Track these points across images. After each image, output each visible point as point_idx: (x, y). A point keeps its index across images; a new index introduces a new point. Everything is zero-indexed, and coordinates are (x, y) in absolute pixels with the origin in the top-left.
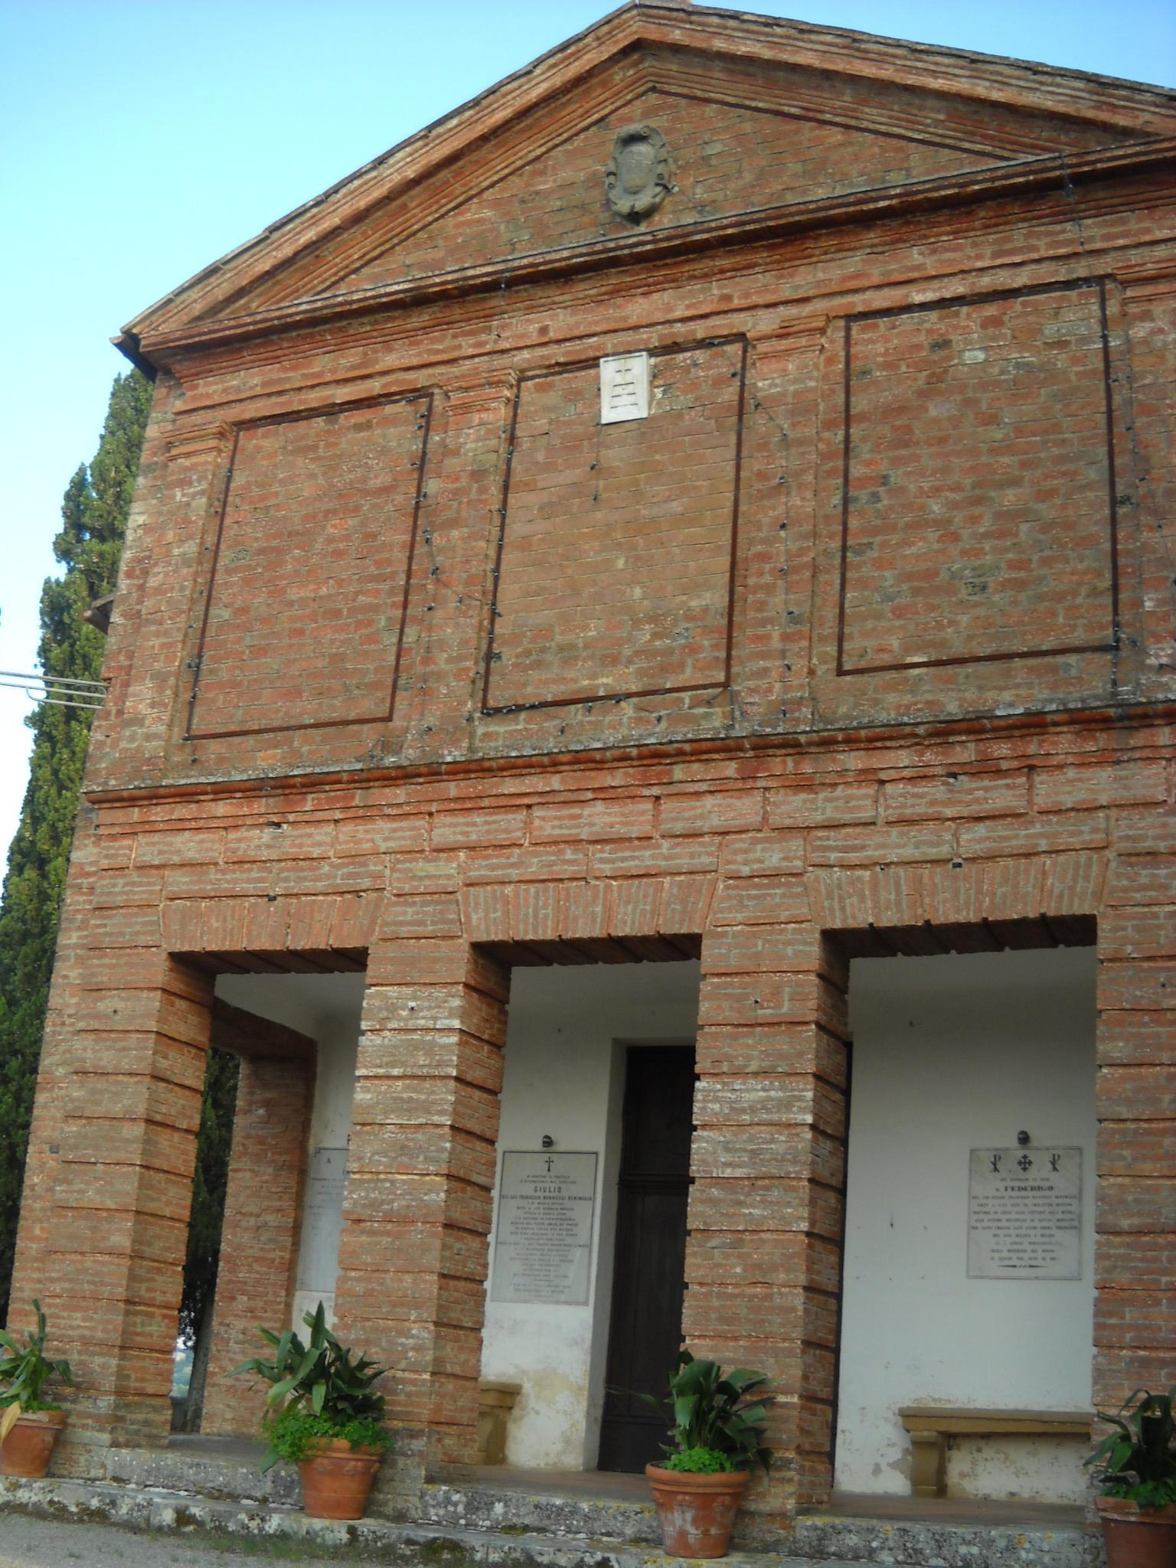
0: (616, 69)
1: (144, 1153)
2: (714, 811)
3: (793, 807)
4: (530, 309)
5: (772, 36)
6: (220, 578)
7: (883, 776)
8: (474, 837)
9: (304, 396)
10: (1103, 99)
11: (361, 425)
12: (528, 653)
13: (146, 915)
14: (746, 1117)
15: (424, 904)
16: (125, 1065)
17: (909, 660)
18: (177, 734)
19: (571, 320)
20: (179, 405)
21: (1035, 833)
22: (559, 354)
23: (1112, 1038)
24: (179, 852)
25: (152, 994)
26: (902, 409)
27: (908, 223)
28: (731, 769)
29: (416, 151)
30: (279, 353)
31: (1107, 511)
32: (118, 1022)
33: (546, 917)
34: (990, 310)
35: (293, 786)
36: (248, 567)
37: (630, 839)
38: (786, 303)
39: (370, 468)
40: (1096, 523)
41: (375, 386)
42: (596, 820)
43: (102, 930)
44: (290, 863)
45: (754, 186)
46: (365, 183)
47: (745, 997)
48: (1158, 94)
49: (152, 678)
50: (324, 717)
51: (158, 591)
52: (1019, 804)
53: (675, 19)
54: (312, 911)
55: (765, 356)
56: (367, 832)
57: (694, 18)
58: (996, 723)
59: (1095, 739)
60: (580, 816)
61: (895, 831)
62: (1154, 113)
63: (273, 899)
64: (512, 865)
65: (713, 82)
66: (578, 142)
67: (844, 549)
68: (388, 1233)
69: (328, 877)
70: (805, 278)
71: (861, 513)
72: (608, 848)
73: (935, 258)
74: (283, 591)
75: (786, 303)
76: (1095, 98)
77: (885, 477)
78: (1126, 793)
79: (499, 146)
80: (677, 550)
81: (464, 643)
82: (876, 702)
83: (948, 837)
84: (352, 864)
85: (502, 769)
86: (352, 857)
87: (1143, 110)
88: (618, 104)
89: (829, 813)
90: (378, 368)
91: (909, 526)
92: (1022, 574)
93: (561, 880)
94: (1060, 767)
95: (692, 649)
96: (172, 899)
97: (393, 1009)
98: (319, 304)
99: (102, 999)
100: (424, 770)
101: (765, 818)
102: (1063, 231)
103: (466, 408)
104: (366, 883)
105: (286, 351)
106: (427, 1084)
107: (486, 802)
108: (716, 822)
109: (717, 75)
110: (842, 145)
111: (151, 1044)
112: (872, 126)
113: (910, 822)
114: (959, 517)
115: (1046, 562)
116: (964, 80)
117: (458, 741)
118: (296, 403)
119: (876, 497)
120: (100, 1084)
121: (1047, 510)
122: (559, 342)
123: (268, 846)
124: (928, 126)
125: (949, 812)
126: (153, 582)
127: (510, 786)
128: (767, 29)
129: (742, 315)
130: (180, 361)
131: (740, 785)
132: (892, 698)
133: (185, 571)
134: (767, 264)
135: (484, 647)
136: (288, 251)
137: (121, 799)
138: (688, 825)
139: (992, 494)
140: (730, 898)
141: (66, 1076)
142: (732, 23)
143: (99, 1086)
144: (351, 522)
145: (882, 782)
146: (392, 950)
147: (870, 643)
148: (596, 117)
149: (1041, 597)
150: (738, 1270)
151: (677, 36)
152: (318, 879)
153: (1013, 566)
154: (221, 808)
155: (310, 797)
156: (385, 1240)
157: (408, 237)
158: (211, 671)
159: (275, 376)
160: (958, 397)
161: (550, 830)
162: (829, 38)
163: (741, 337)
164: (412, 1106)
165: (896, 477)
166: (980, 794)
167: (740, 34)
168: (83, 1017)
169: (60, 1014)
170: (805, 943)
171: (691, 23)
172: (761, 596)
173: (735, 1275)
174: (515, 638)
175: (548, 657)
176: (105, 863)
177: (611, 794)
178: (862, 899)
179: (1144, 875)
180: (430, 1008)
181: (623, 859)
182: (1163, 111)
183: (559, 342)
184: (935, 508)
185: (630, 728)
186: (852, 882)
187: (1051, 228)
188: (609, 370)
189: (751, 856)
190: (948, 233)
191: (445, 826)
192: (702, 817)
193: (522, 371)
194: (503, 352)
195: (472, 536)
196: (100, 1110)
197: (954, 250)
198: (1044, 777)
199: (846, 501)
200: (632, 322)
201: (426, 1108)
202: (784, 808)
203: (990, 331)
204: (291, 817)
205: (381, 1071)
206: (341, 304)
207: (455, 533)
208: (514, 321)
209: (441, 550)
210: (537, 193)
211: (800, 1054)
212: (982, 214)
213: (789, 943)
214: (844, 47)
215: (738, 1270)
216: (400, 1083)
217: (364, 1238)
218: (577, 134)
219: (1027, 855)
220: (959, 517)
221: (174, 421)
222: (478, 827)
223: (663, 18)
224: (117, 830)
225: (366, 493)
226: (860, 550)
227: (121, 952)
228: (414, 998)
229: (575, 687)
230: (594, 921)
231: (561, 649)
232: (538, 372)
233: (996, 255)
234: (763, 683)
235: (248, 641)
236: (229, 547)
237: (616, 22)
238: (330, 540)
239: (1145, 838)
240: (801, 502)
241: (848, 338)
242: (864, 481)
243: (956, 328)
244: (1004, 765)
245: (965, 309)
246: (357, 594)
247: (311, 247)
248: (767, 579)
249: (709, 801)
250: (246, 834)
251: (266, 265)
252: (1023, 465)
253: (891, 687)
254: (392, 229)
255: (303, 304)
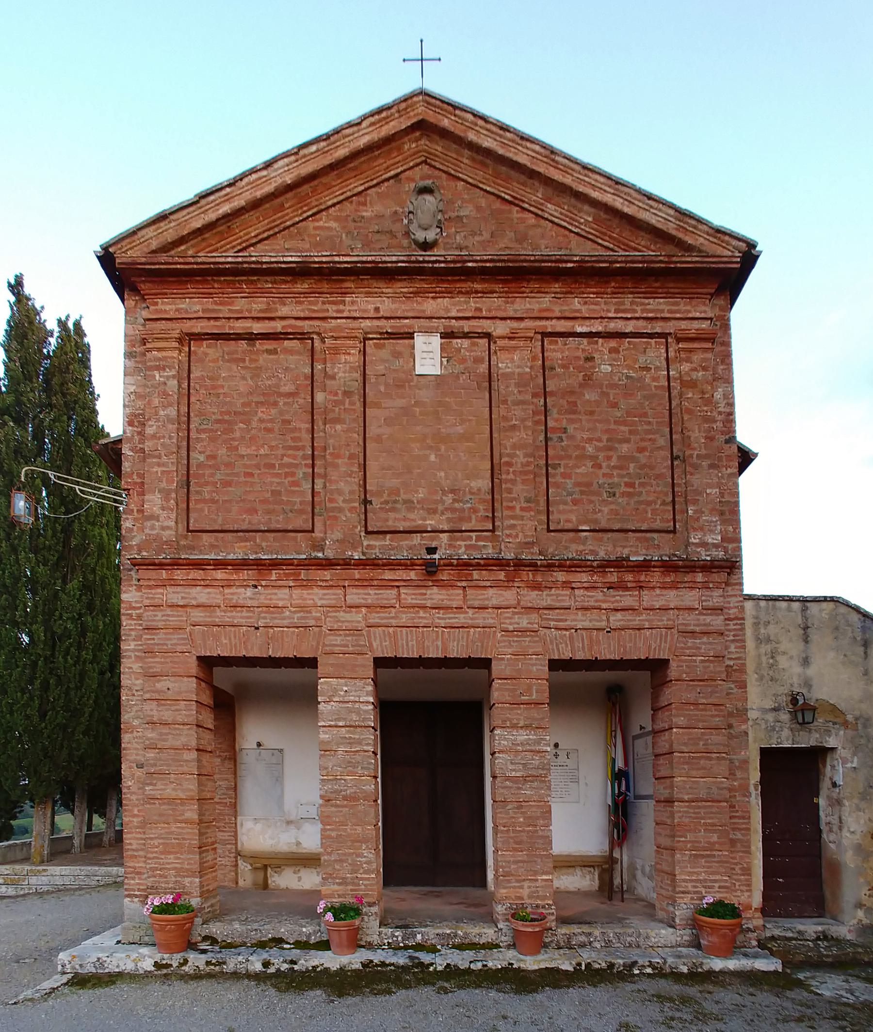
0: (406, 139)
1: (199, 768)
2: (494, 597)
3: (532, 597)
4: (368, 294)
5: (505, 138)
6: (193, 435)
7: (574, 585)
8: (370, 601)
9: (232, 323)
10: (682, 224)
11: (271, 350)
12: (387, 502)
13: (179, 634)
14: (520, 748)
15: (346, 635)
16: (180, 719)
17: (580, 528)
18: (182, 528)
19: (393, 306)
20: (145, 314)
21: (641, 619)
22: (388, 326)
23: (678, 716)
24: (195, 598)
25: (190, 679)
26: (572, 393)
27: (576, 282)
28: (502, 575)
29: (291, 163)
30: (212, 291)
31: (670, 462)
32: (170, 695)
33: (413, 645)
34: (613, 343)
35: (264, 565)
36: (211, 430)
37: (452, 608)
38: (511, 318)
39: (280, 379)
40: (665, 467)
41: (278, 326)
42: (434, 597)
43: (152, 642)
44: (265, 609)
45: (489, 242)
46: (260, 178)
47: (516, 690)
48: (710, 227)
49: (159, 492)
50: (274, 526)
51: (154, 437)
52: (636, 604)
53: (445, 110)
54: (283, 636)
55: (502, 349)
56: (308, 594)
57: (457, 112)
58: (629, 563)
59: (670, 575)
60: (425, 594)
61: (580, 613)
62: (705, 239)
63: (257, 628)
64: (392, 618)
65: (462, 165)
66: (384, 187)
67: (547, 465)
68: (345, 806)
69: (289, 618)
70: (521, 306)
71: (554, 448)
72: (441, 612)
73: (586, 307)
74: (236, 448)
75: (511, 318)
76: (678, 222)
77: (565, 429)
78: (682, 603)
79: (339, 176)
80: (462, 454)
81: (351, 492)
82: (566, 548)
83: (604, 618)
84: (303, 611)
85: (384, 565)
86: (302, 608)
87: (700, 236)
88: (405, 167)
89: (549, 602)
90: (279, 314)
91: (577, 457)
92: (631, 490)
93: (418, 627)
94: (653, 588)
95: (475, 510)
96: (194, 626)
97: (336, 691)
98: (240, 260)
99: (159, 681)
100: (341, 562)
101: (519, 603)
102: (649, 304)
103: (336, 351)
104: (312, 622)
105: (217, 291)
106: (359, 729)
107: (375, 583)
108: (494, 602)
109: (465, 161)
110: (534, 226)
111: (194, 707)
112: (550, 218)
113: (586, 609)
114: (601, 455)
115: (641, 484)
116: (609, 195)
117: (356, 548)
118: (227, 328)
119: (561, 439)
120: (165, 730)
121: (643, 458)
122: (387, 318)
123: (251, 599)
124: (582, 224)
125: (604, 606)
126: (149, 431)
127: (388, 575)
128: (501, 132)
129: (489, 321)
130: (144, 282)
131: (506, 584)
132: (574, 547)
133: (170, 426)
134: (501, 293)
135: (363, 497)
136: (212, 216)
137: (154, 564)
138: (481, 602)
139: (617, 445)
140: (505, 641)
141: (140, 725)
142: (481, 122)
143: (164, 731)
144: (273, 411)
145: (573, 588)
146: (331, 660)
147: (562, 517)
148: (392, 173)
149: (640, 503)
150: (521, 820)
151: (446, 123)
152: (284, 618)
153: (627, 485)
154: (219, 574)
155: (274, 572)
156: (345, 810)
157: (284, 229)
158: (197, 492)
159: (211, 307)
160: (599, 391)
161: (410, 601)
162: (537, 148)
163: (488, 336)
164: (351, 742)
165: (571, 430)
166: (618, 598)
167: (485, 132)
168: (148, 691)
169: (130, 689)
170: (541, 665)
171: (455, 116)
172: (509, 485)
173: (520, 822)
174: (379, 493)
175: (398, 506)
176: (147, 602)
177: (441, 583)
178: (567, 646)
179: (690, 642)
180: (356, 691)
181: (450, 618)
182: (711, 239)
183: (387, 318)
184: (590, 449)
185: (445, 549)
186: (562, 637)
187: (643, 300)
188: (419, 340)
189: (513, 621)
190: (594, 293)
191: (353, 594)
192: (487, 599)
193: (366, 333)
194: (355, 318)
195: (349, 430)
196: (167, 744)
197: (596, 304)
198: (646, 592)
199: (547, 439)
200: (428, 313)
201: (359, 742)
202: (528, 598)
203: (614, 355)
204: (264, 583)
205: (332, 723)
206: (253, 262)
207: (338, 427)
208: (359, 299)
209: (331, 436)
210: (363, 217)
211: (543, 719)
212: (613, 284)
213: (533, 665)
214: (545, 157)
215: (521, 820)
216: (343, 729)
217: (333, 809)
218: (383, 181)
219: (639, 629)
220: (601, 455)
221: (144, 325)
222: (371, 595)
223: (439, 107)
224: (152, 583)
225: (280, 395)
226: (556, 466)
227: (166, 655)
228: (346, 686)
229: (414, 524)
230: (437, 649)
231: (405, 502)
232: (375, 336)
233: (616, 311)
234: (514, 532)
235: (218, 476)
236: (196, 416)
237: (410, 102)
238: (261, 421)
239: (690, 625)
240: (523, 435)
241: (543, 345)
242: (554, 430)
243: (597, 350)
244: (629, 585)
245: (600, 340)
246: (283, 456)
247: (227, 218)
248: (511, 476)
249: (491, 591)
250: (236, 591)
251: (198, 224)
252: (630, 432)
253: (573, 541)
254: (274, 221)
255: (228, 257)
